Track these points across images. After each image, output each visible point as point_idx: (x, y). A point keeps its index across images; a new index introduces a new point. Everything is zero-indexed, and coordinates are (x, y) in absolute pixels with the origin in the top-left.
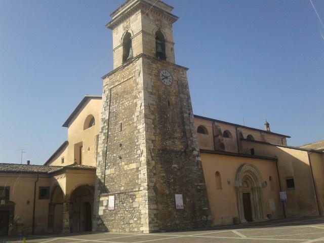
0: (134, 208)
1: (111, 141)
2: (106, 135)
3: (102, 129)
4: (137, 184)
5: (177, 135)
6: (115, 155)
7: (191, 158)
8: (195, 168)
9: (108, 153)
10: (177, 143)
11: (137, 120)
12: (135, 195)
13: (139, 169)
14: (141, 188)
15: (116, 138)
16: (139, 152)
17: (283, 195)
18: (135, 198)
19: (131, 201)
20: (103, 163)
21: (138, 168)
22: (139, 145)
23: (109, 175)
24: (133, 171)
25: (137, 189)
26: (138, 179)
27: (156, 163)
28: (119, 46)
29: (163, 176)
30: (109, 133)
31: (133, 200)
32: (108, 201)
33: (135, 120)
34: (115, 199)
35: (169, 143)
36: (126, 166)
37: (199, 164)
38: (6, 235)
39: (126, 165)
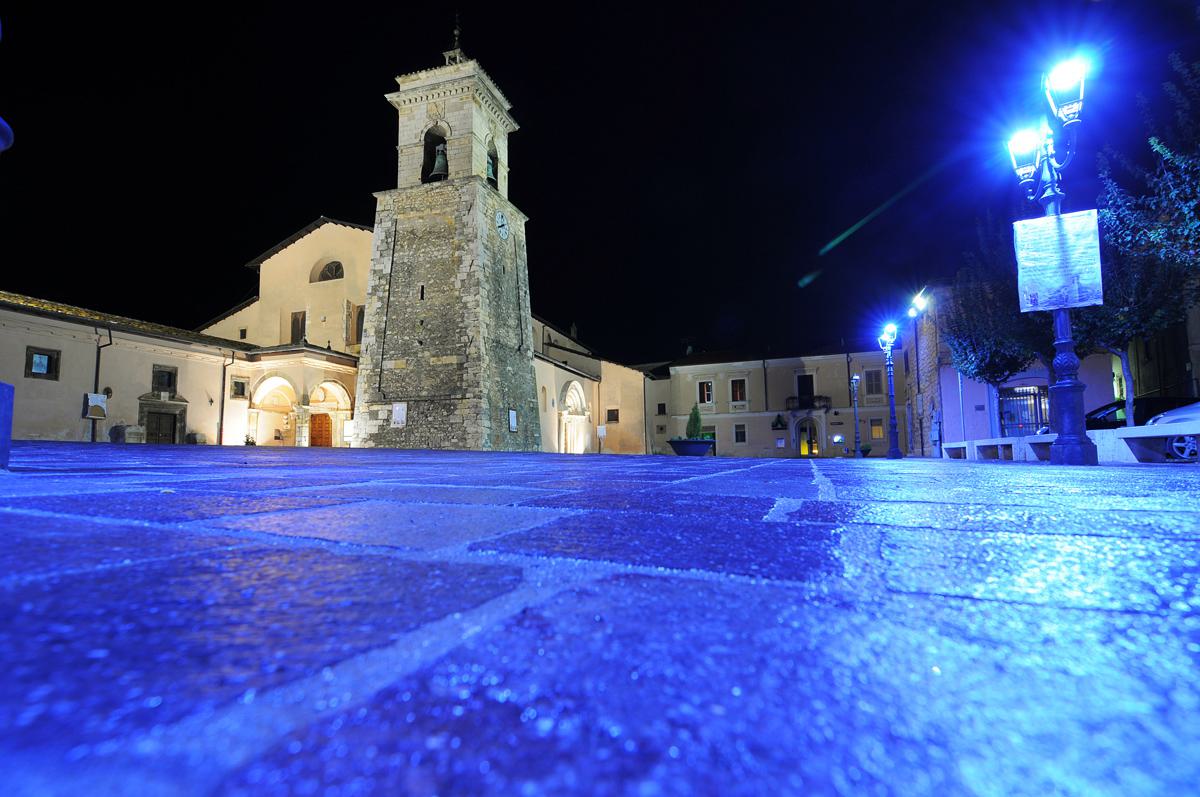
0: (452, 424)
1: (394, 313)
2: (386, 300)
3: (375, 289)
4: (460, 388)
5: (512, 322)
6: (407, 338)
7: (525, 360)
8: (528, 376)
9: (388, 333)
10: (512, 334)
11: (463, 286)
12: (455, 405)
13: (465, 365)
14: (468, 395)
15: (409, 310)
16: (464, 339)
17: (602, 430)
18: (456, 409)
19: (445, 413)
20: (379, 348)
21: (462, 364)
22: (466, 328)
23: (391, 371)
24: (450, 368)
25: (459, 396)
26: (462, 380)
27: (490, 361)
28: (416, 145)
29: (498, 382)
30: (392, 299)
31: (451, 412)
32: (390, 412)
33: (458, 285)
34: (409, 409)
35: (502, 331)
36: (432, 359)
37: (532, 370)
38: (3, 467)
39: (434, 356)
